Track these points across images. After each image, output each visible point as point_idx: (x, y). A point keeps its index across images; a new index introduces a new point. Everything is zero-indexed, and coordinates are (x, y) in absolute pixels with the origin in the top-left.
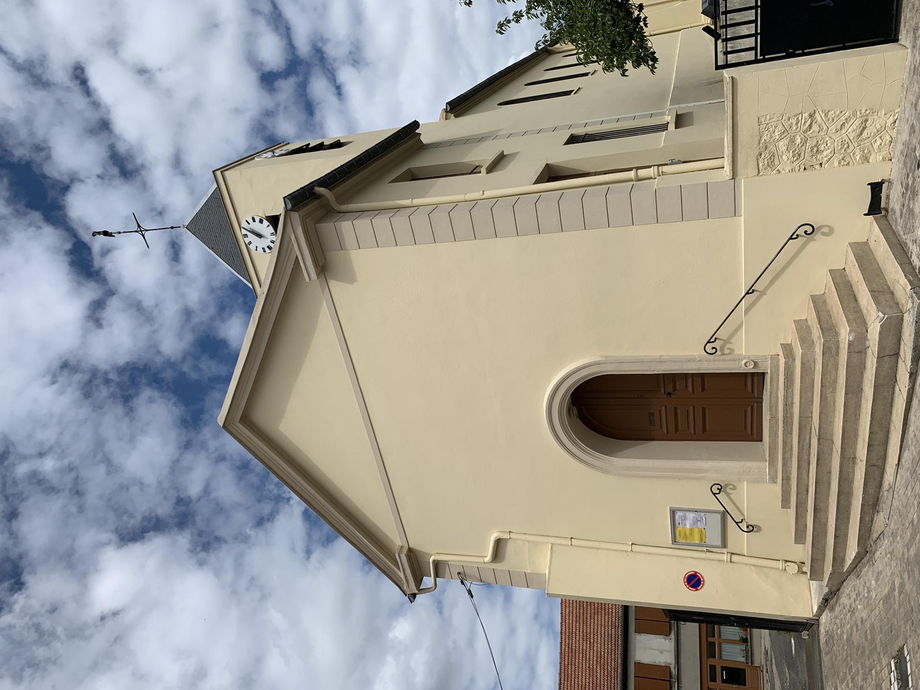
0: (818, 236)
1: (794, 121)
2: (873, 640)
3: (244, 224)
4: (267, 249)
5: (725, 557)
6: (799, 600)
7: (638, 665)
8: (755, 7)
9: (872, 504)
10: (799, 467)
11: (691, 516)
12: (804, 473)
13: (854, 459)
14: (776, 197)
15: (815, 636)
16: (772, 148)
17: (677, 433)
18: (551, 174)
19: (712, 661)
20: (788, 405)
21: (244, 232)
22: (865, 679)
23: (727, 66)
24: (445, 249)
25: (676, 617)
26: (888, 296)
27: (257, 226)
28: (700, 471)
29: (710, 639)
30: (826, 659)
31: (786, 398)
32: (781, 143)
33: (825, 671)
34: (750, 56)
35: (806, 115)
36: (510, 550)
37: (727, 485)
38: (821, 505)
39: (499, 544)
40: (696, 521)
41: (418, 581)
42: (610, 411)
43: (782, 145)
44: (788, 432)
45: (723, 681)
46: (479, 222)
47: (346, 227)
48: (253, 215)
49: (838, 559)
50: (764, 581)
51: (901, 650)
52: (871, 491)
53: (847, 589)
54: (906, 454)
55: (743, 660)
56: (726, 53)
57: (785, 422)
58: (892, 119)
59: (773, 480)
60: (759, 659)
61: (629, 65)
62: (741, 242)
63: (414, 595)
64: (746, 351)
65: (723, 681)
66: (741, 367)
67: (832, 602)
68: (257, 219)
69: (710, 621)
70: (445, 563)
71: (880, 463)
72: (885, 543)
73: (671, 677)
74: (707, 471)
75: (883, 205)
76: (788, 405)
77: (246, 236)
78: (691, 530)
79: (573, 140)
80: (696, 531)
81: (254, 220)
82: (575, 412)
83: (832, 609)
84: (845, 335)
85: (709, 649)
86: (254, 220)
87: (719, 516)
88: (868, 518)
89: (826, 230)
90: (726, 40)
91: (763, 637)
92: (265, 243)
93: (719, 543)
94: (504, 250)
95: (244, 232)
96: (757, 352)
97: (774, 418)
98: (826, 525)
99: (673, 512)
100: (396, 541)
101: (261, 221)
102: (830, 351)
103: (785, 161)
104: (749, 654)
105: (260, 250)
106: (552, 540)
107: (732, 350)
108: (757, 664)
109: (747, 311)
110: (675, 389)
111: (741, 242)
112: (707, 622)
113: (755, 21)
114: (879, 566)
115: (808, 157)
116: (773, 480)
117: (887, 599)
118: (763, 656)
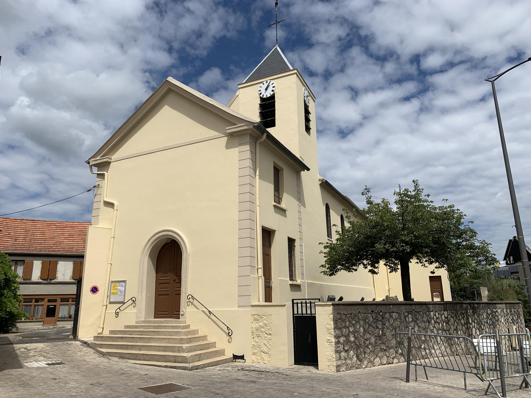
0: (228, 337)
1: (269, 328)
3: (272, 82)
4: (260, 92)
5: (105, 303)
6: (86, 332)
7: (56, 264)
8: (311, 314)
9: (122, 356)
10: (140, 331)
11: (123, 289)
12: (138, 333)
14: (243, 321)
15: (71, 340)
18: (268, 234)
19: (59, 300)
20: (165, 327)
22: (52, 354)
23: (293, 303)
24: (236, 190)
25: (78, 282)
26: (198, 359)
27: (270, 88)
28: (142, 293)
29: (70, 300)
30: (61, 343)
32: (262, 323)
33: (55, 343)
34: (296, 312)
35: (271, 332)
36: (110, 209)
37: (135, 304)
39: (111, 205)
40: (121, 291)
41: (95, 165)
42: (167, 255)
43: (261, 324)
44: (155, 327)
45: (48, 306)
46: (248, 203)
47: (247, 147)
48: (276, 87)
49: (101, 346)
50: (94, 318)
51: (64, 364)
53: (89, 349)
55: (60, 316)
56: (297, 303)
57: (159, 326)
58: (266, 362)
59: (137, 322)
60: (60, 324)
62: (228, 308)
63: (89, 163)
64: (187, 310)
65: (48, 306)
66: (182, 309)
67: (85, 345)
68: (274, 89)
69: (77, 299)
70: (104, 179)
71: (137, 358)
72: (107, 360)
74: (141, 295)
75: (237, 360)
76: (165, 327)
77: (267, 82)
78: (117, 289)
79: (291, 242)
80: (117, 291)
81: (273, 87)
82: (168, 241)
83: (81, 345)
84: (185, 346)
85: (65, 299)
86: (273, 87)
87: (123, 300)
88: (117, 355)
89: (230, 340)
91: (69, 325)
92: (263, 91)
93: (112, 300)
94: (234, 215)
96: (187, 315)
97: (162, 322)
99: (124, 281)
100: (114, 157)
101: (273, 91)
102: (181, 341)
103: (255, 325)
104: (63, 319)
107: (188, 306)
108: (58, 323)
109: (203, 311)
110: (177, 283)
111: (228, 308)
112: (76, 298)
115: (257, 333)
117: (85, 361)
118: (62, 326)
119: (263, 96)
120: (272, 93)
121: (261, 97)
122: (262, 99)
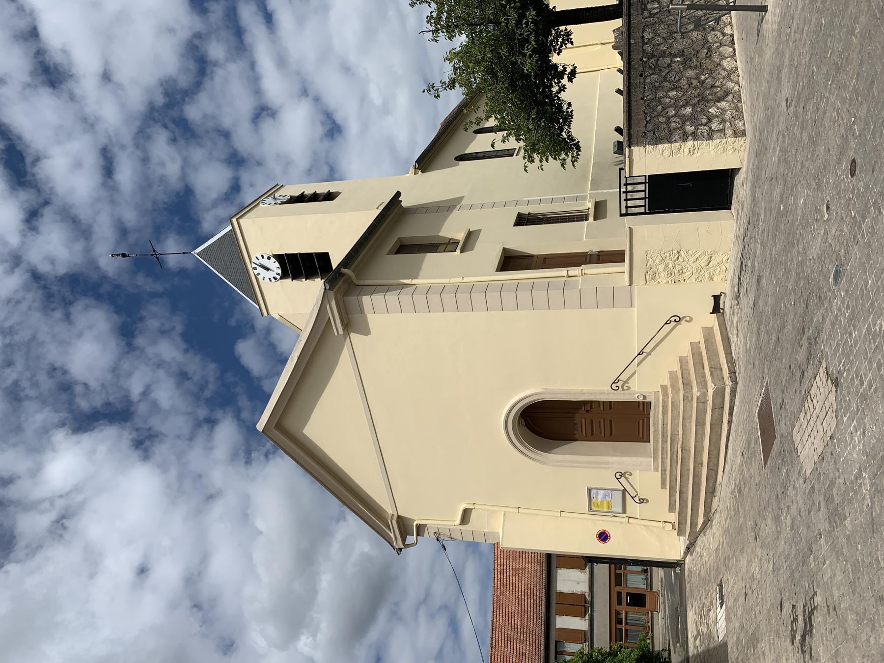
0: (683, 322)
1: (668, 255)
2: (709, 576)
3: (254, 260)
4: (273, 280)
5: (625, 520)
6: (671, 548)
8: (645, 183)
9: (711, 492)
11: (601, 492)
13: (702, 464)
14: (655, 298)
15: (683, 571)
16: (654, 269)
17: (593, 436)
18: (511, 261)
19: (619, 589)
20: (664, 425)
21: (254, 266)
23: (627, 214)
24: (437, 317)
26: (719, 372)
28: (608, 463)
29: (618, 571)
30: (688, 586)
31: (663, 421)
33: (687, 594)
34: (642, 210)
35: (675, 252)
36: (473, 516)
38: (684, 489)
41: (404, 539)
42: (546, 424)
43: (661, 268)
44: (664, 441)
45: (628, 604)
46: (458, 296)
49: (693, 524)
50: (648, 535)
51: (721, 581)
52: (711, 485)
54: (727, 466)
55: (644, 586)
56: (627, 207)
57: (663, 435)
59: (656, 470)
60: (657, 585)
61: (551, 7)
62: (635, 324)
63: (401, 549)
65: (628, 604)
68: (266, 257)
70: (425, 525)
71: (715, 468)
72: (717, 516)
73: (586, 602)
74: (612, 463)
75: (721, 306)
76: (664, 425)
77: (255, 268)
78: (602, 502)
79: (522, 220)
83: (692, 554)
84: (696, 393)
85: (617, 580)
87: (620, 493)
88: (709, 500)
89: (688, 319)
90: (626, 200)
92: (271, 274)
93: (620, 510)
95: (254, 266)
98: (687, 501)
99: (589, 490)
100: (389, 510)
103: (663, 277)
104: (649, 582)
105: (267, 280)
106: (505, 509)
107: (629, 388)
108: (654, 590)
109: (638, 365)
111: (635, 324)
113: (645, 191)
114: (714, 529)
115: (676, 275)
116: (656, 470)
117: (717, 550)
119: (278, 274)
120: (273, 259)
121: (281, 278)
122: (284, 276)
